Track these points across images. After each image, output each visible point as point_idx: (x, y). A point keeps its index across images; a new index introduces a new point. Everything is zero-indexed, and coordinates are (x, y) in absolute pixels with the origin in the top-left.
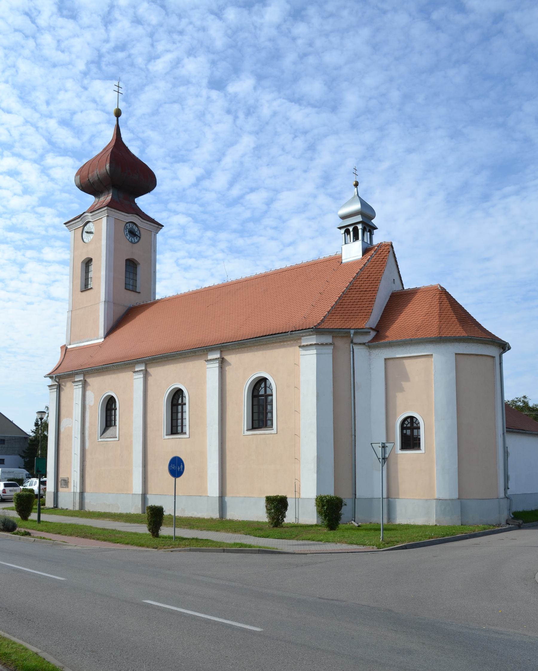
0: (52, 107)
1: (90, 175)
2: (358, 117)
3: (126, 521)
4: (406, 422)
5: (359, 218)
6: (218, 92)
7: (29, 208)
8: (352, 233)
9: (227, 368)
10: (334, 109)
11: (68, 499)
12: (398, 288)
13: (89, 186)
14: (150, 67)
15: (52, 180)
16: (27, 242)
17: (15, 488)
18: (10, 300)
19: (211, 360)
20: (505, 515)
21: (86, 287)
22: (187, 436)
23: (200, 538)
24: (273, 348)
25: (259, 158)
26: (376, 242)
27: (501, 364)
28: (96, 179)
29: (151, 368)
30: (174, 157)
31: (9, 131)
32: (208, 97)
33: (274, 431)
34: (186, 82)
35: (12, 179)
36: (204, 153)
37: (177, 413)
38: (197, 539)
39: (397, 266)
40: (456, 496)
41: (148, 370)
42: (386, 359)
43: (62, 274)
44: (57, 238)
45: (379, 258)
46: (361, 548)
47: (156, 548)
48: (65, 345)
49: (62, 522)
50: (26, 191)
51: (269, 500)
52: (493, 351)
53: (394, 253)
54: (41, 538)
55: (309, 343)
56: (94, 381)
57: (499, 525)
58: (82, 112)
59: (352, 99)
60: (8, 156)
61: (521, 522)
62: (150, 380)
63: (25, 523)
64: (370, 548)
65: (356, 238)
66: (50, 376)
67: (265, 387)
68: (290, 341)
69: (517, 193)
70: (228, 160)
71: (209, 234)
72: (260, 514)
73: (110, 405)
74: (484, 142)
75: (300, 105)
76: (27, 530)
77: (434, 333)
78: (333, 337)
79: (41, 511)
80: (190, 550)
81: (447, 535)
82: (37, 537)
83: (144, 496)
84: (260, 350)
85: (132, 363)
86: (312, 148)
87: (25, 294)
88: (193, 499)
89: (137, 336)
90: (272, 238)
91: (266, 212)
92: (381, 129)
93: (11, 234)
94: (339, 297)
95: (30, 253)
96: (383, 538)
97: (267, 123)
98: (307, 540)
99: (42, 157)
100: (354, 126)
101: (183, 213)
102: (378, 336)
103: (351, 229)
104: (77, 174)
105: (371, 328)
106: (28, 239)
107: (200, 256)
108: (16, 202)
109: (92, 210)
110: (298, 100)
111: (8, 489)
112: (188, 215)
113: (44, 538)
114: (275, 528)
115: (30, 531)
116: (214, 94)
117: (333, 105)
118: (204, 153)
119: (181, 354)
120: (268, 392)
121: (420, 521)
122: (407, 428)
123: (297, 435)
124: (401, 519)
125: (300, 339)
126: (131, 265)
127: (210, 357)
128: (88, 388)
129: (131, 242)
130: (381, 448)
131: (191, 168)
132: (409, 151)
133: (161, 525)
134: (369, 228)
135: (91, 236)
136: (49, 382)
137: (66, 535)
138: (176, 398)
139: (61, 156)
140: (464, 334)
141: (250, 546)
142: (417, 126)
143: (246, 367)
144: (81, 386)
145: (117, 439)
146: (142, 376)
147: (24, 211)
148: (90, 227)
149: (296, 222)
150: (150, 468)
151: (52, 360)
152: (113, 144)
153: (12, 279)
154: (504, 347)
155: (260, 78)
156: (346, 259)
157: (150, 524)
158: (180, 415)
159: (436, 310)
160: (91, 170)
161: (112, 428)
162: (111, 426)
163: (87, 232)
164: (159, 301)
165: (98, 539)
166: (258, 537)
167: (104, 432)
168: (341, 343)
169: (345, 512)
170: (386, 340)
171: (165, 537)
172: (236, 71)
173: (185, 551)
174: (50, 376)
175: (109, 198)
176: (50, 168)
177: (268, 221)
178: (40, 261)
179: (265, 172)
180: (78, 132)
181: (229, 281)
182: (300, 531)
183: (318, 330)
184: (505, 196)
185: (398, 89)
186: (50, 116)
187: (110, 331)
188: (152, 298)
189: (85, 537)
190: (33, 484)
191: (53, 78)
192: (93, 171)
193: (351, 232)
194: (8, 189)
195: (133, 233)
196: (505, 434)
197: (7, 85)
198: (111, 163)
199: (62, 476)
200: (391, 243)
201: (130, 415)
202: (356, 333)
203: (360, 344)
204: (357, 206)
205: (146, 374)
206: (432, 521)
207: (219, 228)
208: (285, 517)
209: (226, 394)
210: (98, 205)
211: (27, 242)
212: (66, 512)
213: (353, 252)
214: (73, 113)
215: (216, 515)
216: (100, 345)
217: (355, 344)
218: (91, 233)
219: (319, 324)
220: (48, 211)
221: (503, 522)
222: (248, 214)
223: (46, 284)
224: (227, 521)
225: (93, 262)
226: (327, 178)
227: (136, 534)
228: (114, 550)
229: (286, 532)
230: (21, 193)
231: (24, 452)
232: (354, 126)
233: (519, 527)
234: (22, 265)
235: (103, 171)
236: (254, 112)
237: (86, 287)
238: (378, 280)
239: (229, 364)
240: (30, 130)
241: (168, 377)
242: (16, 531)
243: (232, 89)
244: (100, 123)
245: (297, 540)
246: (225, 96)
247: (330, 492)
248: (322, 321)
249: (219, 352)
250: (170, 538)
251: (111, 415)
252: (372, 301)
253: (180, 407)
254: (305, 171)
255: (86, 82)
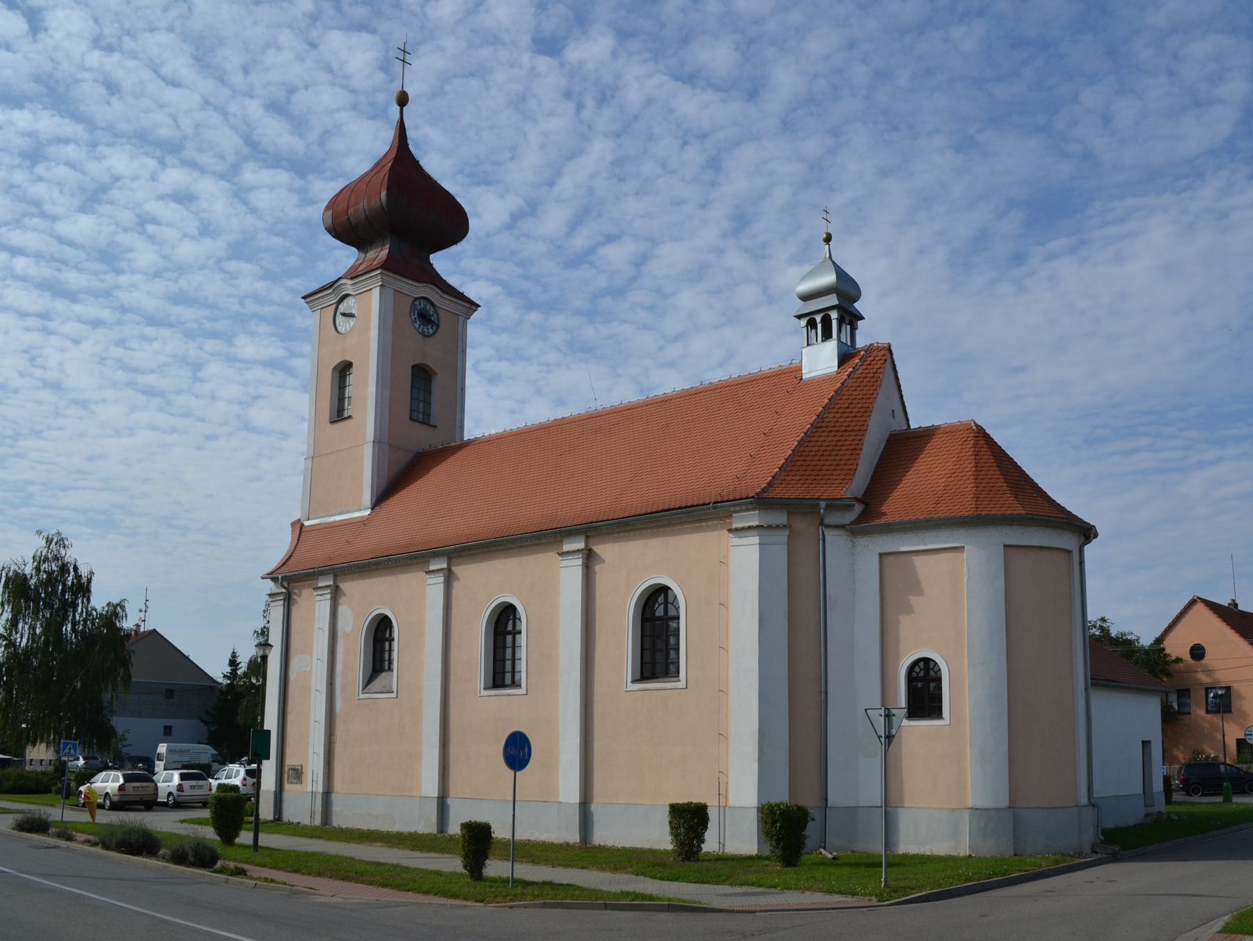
0: (254, 78)
1: (351, 211)
2: (795, 110)
3: (413, 849)
4: (917, 669)
5: (832, 300)
6: (548, 58)
7: (211, 262)
8: (819, 326)
9: (598, 568)
10: (752, 95)
11: (301, 804)
12: (898, 426)
13: (347, 227)
14: (430, 10)
15: (254, 211)
16: (207, 325)
17: (201, 783)
18: (174, 430)
19: (568, 553)
20: (1090, 836)
21: (339, 414)
22: (522, 691)
23: (565, 882)
24: (681, 532)
25: (621, 180)
26: (861, 342)
27: (1082, 563)
28: (362, 217)
29: (458, 564)
30: (470, 175)
31: (175, 119)
32: (533, 68)
33: (682, 684)
34: (494, 39)
35: (180, 207)
36: (524, 170)
37: (504, 648)
38: (550, 883)
39: (899, 386)
40: (1004, 802)
41: (453, 568)
42: (881, 555)
43: (270, 385)
44: (262, 319)
45: (869, 370)
46: (836, 899)
47: (482, 901)
48: (299, 520)
49: (298, 849)
50: (207, 230)
51: (677, 811)
52: (1066, 541)
53: (893, 362)
54: (266, 880)
55: (746, 525)
56: (352, 588)
57: (1080, 854)
58: (306, 88)
59: (786, 79)
60: (173, 166)
61: (1117, 848)
62: (457, 587)
63: (229, 851)
64: (865, 901)
65: (827, 335)
66: (272, 576)
67: (666, 603)
68: (710, 520)
69: (1073, 251)
70: (566, 185)
71: (534, 316)
72: (657, 835)
73: (381, 631)
74: (1016, 158)
75: (694, 86)
76: (239, 865)
77: (966, 507)
78: (789, 514)
79: (261, 827)
80: (545, 906)
81: (995, 874)
82: (259, 879)
83: (442, 801)
84: (657, 536)
85: (423, 556)
86: (714, 164)
87: (202, 420)
88: (541, 808)
89: (431, 506)
90: (645, 327)
91: (634, 279)
92: (835, 132)
93: (178, 310)
94: (799, 442)
95: (211, 345)
96: (886, 881)
97: (636, 117)
98: (748, 885)
99: (235, 169)
100: (787, 126)
101: (487, 279)
102: (868, 514)
103: (818, 318)
104: (327, 208)
105: (856, 499)
106: (209, 319)
107: (516, 356)
108: (187, 251)
109: (353, 274)
110: (689, 78)
111: (187, 784)
112: (499, 282)
113: (272, 881)
114: (687, 863)
115: (245, 866)
116: (543, 63)
117: (752, 88)
118: (524, 170)
119: (514, 541)
120: (672, 613)
121: (941, 848)
122: (918, 679)
123: (723, 692)
124: (907, 845)
125: (731, 516)
126: (422, 376)
127: (566, 548)
128: (342, 600)
129: (423, 334)
130: (882, 719)
131: (502, 196)
132: (884, 173)
133: (486, 858)
134: (851, 318)
135: (352, 321)
136: (270, 586)
137: (309, 874)
138: (504, 622)
139: (267, 167)
140: (1020, 510)
141: (651, 898)
142: (896, 129)
143: (632, 565)
144: (329, 596)
145: (394, 695)
146: (441, 579)
147: (202, 267)
148: (349, 305)
149: (686, 299)
150: (453, 749)
151: (277, 548)
152: (393, 155)
153: (179, 392)
154: (1087, 533)
155: (623, 35)
156: (808, 373)
157: (466, 857)
158: (509, 651)
159: (970, 466)
160: (352, 200)
161: (384, 674)
162: (382, 670)
163: (344, 314)
164: (470, 442)
165: (371, 883)
166: (660, 879)
167: (369, 680)
168: (803, 525)
169: (811, 830)
170: (883, 521)
171: (494, 880)
172: (581, 22)
173: (535, 906)
174: (272, 576)
175: (385, 253)
176: (250, 189)
177: (636, 296)
178: (231, 359)
179: (632, 206)
180: (299, 124)
181: (599, 408)
182: (730, 868)
183: (762, 501)
184: (1051, 257)
185: (864, 61)
186: (250, 95)
187: (382, 496)
188: (457, 436)
189: (346, 878)
190: (235, 775)
191: (255, 23)
192: (356, 203)
193: (817, 324)
194: (172, 226)
195: (426, 318)
196: (1090, 690)
197: (172, 35)
198: (389, 189)
199: (290, 761)
200: (889, 345)
201: (418, 652)
202: (829, 508)
203: (836, 527)
204: (829, 278)
205: (449, 577)
206: (964, 850)
207: (552, 307)
208: (703, 842)
209: (594, 613)
210: (364, 265)
211: (207, 325)
212: (297, 830)
213: (821, 360)
214: (292, 90)
215: (574, 837)
216: (363, 522)
217: (828, 526)
218: (351, 315)
219: (764, 490)
220: (245, 267)
221: (1087, 849)
222: (602, 282)
223: (240, 403)
224: (594, 847)
225: (354, 369)
226: (741, 221)
227: (438, 873)
228: (405, 904)
229: (708, 871)
230: (196, 232)
231: (208, 713)
232: (787, 126)
233: (1114, 858)
234: (197, 367)
235: (375, 203)
236: (612, 97)
237: (339, 414)
238: (866, 412)
239: (602, 561)
240: (215, 118)
241: (488, 583)
242: (219, 864)
243: (576, 53)
244: (338, 110)
245: (731, 885)
246: (562, 65)
247: (781, 796)
248: (770, 484)
249: (583, 538)
250: (505, 881)
251: (383, 651)
252: (857, 449)
253: (509, 638)
254: (703, 206)
255: (315, 34)
